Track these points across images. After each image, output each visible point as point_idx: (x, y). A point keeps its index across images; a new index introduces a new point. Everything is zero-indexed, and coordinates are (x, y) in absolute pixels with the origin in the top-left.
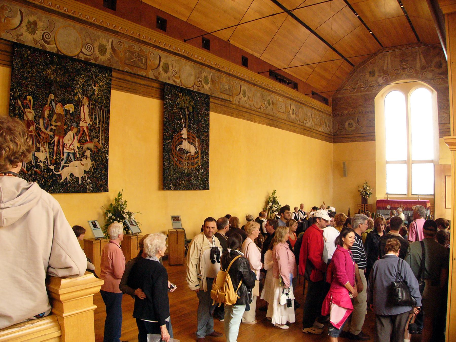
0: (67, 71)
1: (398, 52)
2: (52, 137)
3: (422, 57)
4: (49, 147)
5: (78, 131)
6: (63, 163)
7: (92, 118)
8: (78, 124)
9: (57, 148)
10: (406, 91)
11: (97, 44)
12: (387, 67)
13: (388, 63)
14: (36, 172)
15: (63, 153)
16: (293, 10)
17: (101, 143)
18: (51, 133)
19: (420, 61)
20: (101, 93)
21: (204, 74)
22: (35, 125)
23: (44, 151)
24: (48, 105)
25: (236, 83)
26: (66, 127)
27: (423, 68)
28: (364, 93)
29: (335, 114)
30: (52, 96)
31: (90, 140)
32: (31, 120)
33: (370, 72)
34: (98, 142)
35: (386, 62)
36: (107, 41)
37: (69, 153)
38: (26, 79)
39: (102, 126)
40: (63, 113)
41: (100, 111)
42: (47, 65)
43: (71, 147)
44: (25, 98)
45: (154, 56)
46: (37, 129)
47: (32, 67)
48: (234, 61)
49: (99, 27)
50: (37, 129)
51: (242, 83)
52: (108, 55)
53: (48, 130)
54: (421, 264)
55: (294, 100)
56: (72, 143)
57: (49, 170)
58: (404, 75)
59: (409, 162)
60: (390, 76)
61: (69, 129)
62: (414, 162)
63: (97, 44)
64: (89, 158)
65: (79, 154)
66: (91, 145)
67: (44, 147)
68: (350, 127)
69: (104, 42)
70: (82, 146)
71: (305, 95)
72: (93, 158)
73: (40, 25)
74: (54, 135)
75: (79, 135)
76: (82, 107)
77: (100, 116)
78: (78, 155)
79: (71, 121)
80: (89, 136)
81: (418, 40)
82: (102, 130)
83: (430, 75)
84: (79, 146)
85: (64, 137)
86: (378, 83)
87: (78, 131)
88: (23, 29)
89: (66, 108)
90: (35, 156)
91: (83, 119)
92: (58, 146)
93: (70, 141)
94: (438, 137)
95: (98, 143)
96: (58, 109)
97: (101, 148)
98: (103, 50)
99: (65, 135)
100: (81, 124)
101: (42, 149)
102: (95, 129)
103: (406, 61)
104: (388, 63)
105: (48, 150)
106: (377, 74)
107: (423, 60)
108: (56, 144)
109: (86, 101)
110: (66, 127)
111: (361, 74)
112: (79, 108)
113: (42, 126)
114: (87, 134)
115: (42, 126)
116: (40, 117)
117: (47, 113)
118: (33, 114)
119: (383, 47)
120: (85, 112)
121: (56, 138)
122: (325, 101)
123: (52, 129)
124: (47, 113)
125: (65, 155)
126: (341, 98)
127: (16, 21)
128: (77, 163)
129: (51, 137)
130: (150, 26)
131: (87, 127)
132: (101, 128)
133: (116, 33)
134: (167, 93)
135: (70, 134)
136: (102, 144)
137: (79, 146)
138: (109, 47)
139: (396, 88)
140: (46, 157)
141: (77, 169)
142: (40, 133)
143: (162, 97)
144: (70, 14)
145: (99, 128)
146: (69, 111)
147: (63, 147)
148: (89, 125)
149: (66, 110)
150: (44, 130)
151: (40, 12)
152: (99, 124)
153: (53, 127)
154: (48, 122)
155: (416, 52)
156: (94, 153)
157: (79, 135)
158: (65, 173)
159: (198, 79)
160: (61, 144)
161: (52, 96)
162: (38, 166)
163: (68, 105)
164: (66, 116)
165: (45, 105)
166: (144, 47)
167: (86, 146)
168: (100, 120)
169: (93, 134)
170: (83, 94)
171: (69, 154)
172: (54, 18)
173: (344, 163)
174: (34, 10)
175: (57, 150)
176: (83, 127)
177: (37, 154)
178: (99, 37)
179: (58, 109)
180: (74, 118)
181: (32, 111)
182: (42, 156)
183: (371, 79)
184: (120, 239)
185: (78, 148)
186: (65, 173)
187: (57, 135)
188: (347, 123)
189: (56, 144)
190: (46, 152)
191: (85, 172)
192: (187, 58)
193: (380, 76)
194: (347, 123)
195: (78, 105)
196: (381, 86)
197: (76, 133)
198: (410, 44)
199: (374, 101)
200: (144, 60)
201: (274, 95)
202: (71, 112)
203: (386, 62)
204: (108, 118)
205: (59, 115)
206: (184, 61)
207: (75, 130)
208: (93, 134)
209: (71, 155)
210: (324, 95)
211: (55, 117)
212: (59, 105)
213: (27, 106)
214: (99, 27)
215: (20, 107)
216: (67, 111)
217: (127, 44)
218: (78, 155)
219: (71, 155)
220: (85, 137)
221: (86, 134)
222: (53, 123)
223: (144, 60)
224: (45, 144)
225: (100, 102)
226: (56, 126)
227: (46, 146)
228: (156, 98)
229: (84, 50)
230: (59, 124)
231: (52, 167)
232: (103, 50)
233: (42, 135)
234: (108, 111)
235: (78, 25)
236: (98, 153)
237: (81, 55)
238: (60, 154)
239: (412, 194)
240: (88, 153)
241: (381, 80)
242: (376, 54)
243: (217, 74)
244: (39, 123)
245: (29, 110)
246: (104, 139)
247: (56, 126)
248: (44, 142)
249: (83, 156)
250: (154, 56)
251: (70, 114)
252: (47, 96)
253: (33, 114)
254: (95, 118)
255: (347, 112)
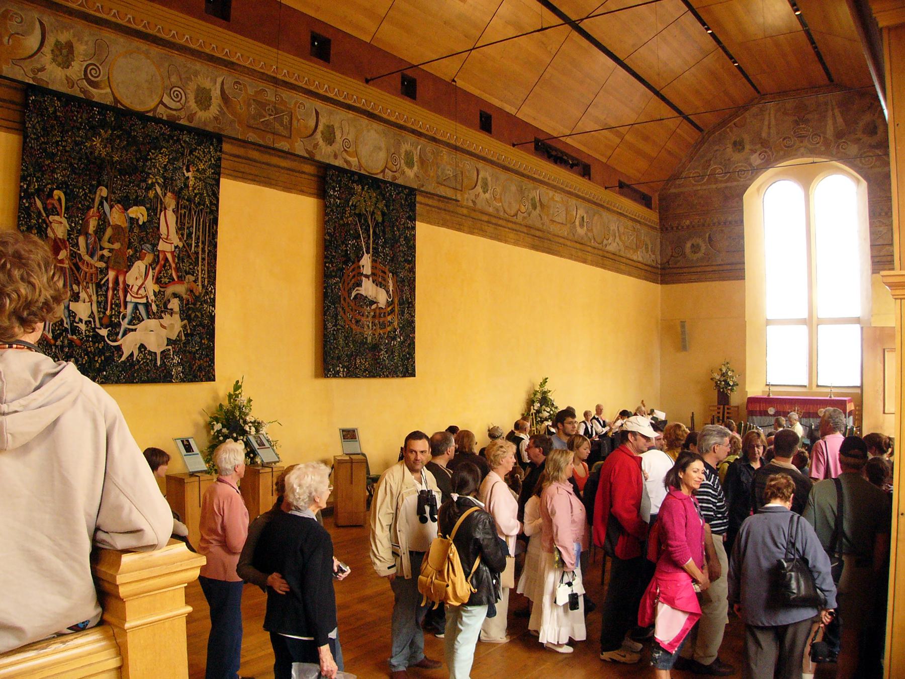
0: (133, 141)
1: (790, 104)
2: (104, 272)
3: (837, 112)
4: (97, 292)
5: (156, 261)
6: (125, 324)
7: (183, 235)
8: (155, 246)
9: (114, 294)
10: (806, 181)
11: (192, 87)
12: (769, 134)
13: (769, 124)
14: (71, 342)
15: (126, 303)
16: (582, 20)
17: (200, 284)
18: (102, 265)
19: (833, 122)
20: (200, 184)
21: (405, 147)
22: (69, 247)
23: (87, 300)
24: (95, 209)
25: (468, 164)
26: (130, 251)
27: (839, 135)
28: (723, 185)
29: (664, 227)
30: (104, 192)
31: (178, 277)
32: (61, 237)
33: (735, 144)
34: (195, 281)
35: (766, 123)
36: (213, 81)
37: (136, 304)
38: (52, 156)
39: (203, 250)
40: (125, 225)
41: (198, 221)
42: (94, 130)
43: (142, 292)
44: (50, 195)
45: (305, 111)
46: (74, 256)
47: (63, 132)
48: (465, 122)
49: (197, 54)
50: (74, 256)
51: (480, 164)
52: (214, 110)
53: (96, 258)
54: (836, 525)
55: (584, 199)
56: (143, 284)
57: (97, 338)
58: (802, 150)
59: (811, 323)
60: (774, 151)
61: (138, 256)
62: (821, 322)
63: (192, 87)
64: (176, 313)
65: (157, 306)
66: (181, 289)
67: (87, 293)
68: (695, 253)
69: (207, 84)
70: (162, 290)
71: (606, 188)
72: (185, 314)
73: (80, 49)
74: (107, 268)
75: (157, 269)
76: (163, 213)
77: (198, 229)
78: (154, 308)
79: (141, 240)
80: (178, 270)
81: (831, 79)
82: (203, 259)
83: (853, 149)
84: (157, 290)
85: (127, 272)
86: (750, 165)
87: (154, 259)
88: (46, 58)
89: (131, 215)
90: (69, 310)
91: (164, 236)
92: (114, 289)
93: (140, 279)
94: (870, 272)
95: (194, 285)
96: (116, 217)
97: (200, 294)
98: (203, 99)
99: (129, 267)
100: (162, 246)
101: (83, 295)
102: (189, 256)
103: (806, 121)
104: (769, 124)
105: (94, 298)
106: (748, 147)
107: (840, 120)
108: (111, 285)
109: (170, 201)
110: (131, 253)
111: (716, 148)
112: (156, 215)
113: (82, 250)
114: (173, 265)
115: (82, 250)
116: (79, 233)
117: (93, 225)
118: (65, 227)
119: (759, 94)
120: (168, 222)
121: (111, 275)
122: (645, 200)
123: (102, 256)
124: (93, 225)
125: (130, 307)
126: (677, 195)
127: (32, 42)
128: (153, 323)
129: (101, 271)
130: (297, 52)
131: (172, 253)
132: (200, 255)
133: (230, 65)
134: (331, 184)
135: (139, 266)
136: (203, 286)
137: (157, 290)
138: (216, 93)
139: (787, 174)
140: (92, 312)
141: (152, 336)
142: (80, 264)
143: (322, 193)
144: (140, 28)
145: (197, 253)
146: (138, 220)
147: (126, 292)
148: (176, 247)
149: (131, 219)
150: (87, 258)
151: (80, 25)
152: (197, 246)
153: (106, 253)
154: (95, 242)
155: (826, 104)
156: (186, 305)
157: (157, 269)
158: (129, 344)
159: (392, 156)
160: (121, 285)
161: (104, 192)
162: (75, 330)
163: (135, 208)
164: (131, 230)
165: (89, 208)
166: (285, 94)
167: (170, 290)
168: (198, 238)
169: (185, 266)
170: (164, 187)
171: (136, 306)
172: (107, 35)
173: (683, 324)
174: (67, 20)
175: (113, 298)
176: (164, 252)
177: (73, 306)
178: (196, 74)
179: (116, 217)
180: (147, 234)
181: (64, 221)
182: (82, 310)
183: (737, 157)
184: (239, 475)
185: (155, 294)
186: (129, 344)
187: (113, 269)
188: (688, 245)
189: (111, 285)
190: (91, 301)
191: (170, 342)
192: (371, 116)
193: (753, 151)
194: (688, 245)
195: (155, 209)
196: (756, 171)
197: (150, 265)
198: (813, 88)
199: (742, 200)
200: (286, 120)
201: (543, 189)
202: (141, 223)
203: (766, 123)
204: (214, 235)
205: (117, 228)
206: (364, 121)
207: (149, 258)
208: (185, 266)
209: (141, 308)
210: (644, 189)
211: (109, 232)
212: (118, 208)
213: (54, 211)
214: (197, 54)
215: (40, 212)
216: (133, 221)
217: (251, 87)
218: (154, 308)
219: (141, 308)
220: (170, 272)
221: (170, 265)
222: (106, 245)
223: (286, 120)
224: (90, 285)
225: (199, 203)
226: (111, 250)
227: (91, 290)
228: (310, 194)
229: (166, 100)
230: (117, 246)
231: (104, 332)
232: (203, 99)
233: (84, 268)
234: (215, 221)
235: (155, 50)
236: (195, 304)
237: (161, 110)
238: (118, 305)
239: (818, 386)
240: (175, 304)
241: (756, 160)
242: (745, 108)
243: (430, 147)
244: (77, 244)
245: (57, 218)
246: (206, 276)
247: (111, 250)
248: (87, 283)
249: (164, 309)
250: (305, 111)
251: (140, 226)
252: (93, 190)
253: (65, 227)
254: (189, 235)
255: (688, 222)
